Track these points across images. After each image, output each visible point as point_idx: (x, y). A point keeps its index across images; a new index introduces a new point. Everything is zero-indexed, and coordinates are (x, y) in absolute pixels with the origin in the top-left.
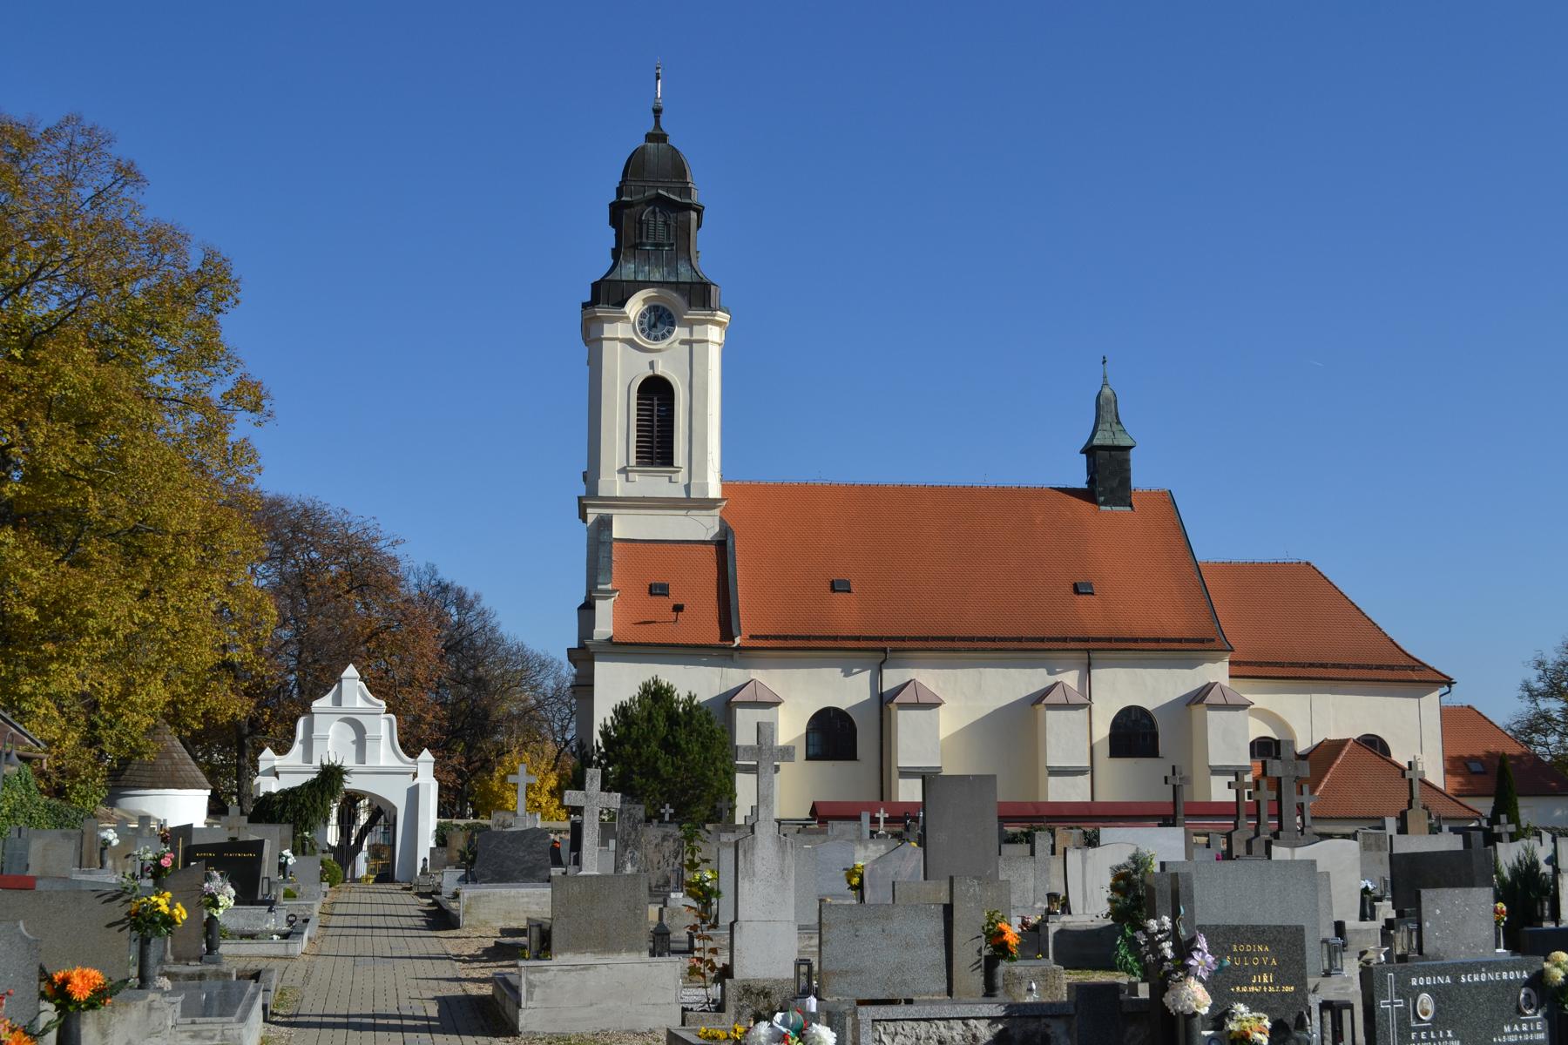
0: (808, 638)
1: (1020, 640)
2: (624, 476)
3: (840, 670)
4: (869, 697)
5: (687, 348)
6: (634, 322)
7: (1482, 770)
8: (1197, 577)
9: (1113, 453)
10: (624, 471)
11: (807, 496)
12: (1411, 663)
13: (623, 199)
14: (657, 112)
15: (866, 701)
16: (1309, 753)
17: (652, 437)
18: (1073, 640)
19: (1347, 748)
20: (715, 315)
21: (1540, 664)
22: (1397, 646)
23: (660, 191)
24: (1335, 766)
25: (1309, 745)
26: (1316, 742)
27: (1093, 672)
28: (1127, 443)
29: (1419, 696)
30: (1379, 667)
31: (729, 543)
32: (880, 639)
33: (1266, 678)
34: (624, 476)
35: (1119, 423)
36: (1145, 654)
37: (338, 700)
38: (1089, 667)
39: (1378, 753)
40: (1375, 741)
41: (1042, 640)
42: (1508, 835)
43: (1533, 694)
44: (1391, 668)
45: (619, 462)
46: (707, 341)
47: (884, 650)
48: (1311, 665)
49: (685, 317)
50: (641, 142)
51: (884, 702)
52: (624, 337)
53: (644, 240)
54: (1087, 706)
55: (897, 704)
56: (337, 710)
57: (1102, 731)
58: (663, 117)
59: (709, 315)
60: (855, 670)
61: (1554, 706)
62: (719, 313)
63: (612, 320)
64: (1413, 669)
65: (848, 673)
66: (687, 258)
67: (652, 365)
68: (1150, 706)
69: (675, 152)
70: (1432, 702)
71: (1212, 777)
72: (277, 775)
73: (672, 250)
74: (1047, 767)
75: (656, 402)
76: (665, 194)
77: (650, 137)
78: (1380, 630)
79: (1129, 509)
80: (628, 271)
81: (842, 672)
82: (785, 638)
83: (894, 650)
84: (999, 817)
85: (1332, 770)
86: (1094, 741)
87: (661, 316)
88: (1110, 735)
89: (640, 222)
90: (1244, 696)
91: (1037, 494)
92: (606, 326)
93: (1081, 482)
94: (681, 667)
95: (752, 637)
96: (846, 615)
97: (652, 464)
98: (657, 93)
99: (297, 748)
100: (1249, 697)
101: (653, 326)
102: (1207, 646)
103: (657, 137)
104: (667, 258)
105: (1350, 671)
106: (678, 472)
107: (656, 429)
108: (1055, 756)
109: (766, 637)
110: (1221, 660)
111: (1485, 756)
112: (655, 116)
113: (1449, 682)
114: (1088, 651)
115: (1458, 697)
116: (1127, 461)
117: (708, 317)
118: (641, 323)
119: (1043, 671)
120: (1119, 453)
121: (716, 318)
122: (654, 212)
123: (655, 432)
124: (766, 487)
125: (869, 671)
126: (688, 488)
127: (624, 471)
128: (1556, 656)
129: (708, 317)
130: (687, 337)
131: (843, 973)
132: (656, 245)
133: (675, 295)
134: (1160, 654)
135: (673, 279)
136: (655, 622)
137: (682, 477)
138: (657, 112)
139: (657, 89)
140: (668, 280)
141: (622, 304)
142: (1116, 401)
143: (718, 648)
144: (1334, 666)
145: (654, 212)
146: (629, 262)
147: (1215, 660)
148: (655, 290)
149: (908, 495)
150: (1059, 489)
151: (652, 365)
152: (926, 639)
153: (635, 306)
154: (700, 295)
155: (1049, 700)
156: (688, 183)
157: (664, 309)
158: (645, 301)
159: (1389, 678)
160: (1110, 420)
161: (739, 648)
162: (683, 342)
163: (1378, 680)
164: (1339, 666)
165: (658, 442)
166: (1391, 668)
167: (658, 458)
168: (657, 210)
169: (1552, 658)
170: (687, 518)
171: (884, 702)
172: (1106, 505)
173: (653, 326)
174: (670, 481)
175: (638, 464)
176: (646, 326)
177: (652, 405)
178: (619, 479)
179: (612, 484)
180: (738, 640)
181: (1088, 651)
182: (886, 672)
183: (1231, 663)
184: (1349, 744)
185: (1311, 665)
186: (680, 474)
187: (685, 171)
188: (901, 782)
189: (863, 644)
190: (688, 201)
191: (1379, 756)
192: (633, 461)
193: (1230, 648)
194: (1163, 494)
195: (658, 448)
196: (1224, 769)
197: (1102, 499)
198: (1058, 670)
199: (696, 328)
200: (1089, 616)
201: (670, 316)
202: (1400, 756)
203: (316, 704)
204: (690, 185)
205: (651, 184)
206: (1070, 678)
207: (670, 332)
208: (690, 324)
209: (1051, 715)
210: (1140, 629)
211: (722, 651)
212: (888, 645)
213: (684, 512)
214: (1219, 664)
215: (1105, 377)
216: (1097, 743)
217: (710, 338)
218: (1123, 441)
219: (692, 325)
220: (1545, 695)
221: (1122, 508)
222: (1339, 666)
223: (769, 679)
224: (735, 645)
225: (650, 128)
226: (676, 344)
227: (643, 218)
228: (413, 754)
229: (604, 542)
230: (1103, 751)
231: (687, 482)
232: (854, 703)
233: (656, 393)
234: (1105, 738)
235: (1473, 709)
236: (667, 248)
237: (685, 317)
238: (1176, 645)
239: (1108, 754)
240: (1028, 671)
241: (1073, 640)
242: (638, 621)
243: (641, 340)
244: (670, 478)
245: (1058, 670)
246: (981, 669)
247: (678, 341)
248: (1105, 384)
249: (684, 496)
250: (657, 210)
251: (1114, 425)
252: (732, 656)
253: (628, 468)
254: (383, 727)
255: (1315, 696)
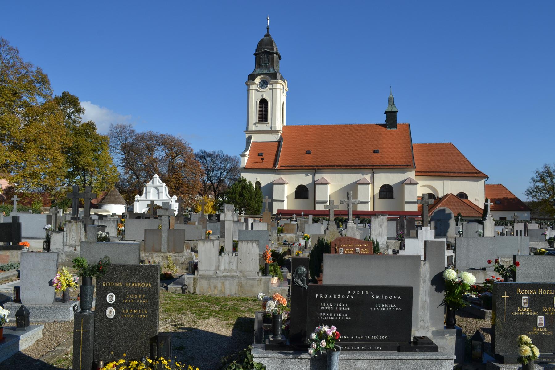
1: (354, 166)
5: (271, 90)
8: (411, 148)
10: (255, 124)
11: (306, 129)
14: (268, 29)
17: (262, 116)
18: (369, 166)
22: (473, 167)
23: (266, 50)
24: (443, 201)
26: (445, 195)
27: (374, 174)
29: (478, 181)
30: (465, 173)
31: (281, 142)
32: (315, 166)
33: (429, 176)
35: (394, 105)
36: (389, 170)
37: (153, 183)
38: (373, 173)
41: (360, 166)
42: (156, 227)
45: (254, 122)
47: (315, 169)
48: (444, 172)
50: (263, 37)
51: (315, 184)
53: (262, 63)
56: (153, 185)
57: (377, 191)
58: (269, 30)
63: (252, 84)
64: (476, 173)
65: (306, 175)
67: (262, 95)
68: (391, 184)
69: (271, 38)
70: (482, 183)
72: (139, 201)
75: (263, 105)
76: (267, 50)
77: (266, 36)
80: (258, 71)
82: (289, 166)
83: (317, 169)
84: (335, 214)
86: (374, 194)
88: (379, 192)
89: (261, 58)
91: (370, 126)
92: (250, 86)
93: (383, 122)
94: (263, 174)
95: (281, 166)
96: (308, 160)
97: (262, 122)
99: (144, 195)
100: (418, 181)
101: (262, 85)
102: (408, 167)
103: (267, 35)
105: (456, 174)
109: (284, 166)
110: (413, 171)
113: (487, 177)
114: (373, 169)
115: (491, 181)
116: (396, 115)
118: (259, 85)
119: (361, 174)
122: (264, 55)
124: (296, 127)
126: (271, 128)
127: (255, 124)
130: (271, 88)
133: (267, 77)
137: (270, 125)
138: (268, 29)
141: (254, 80)
142: (393, 99)
144: (451, 172)
147: (411, 171)
149: (333, 127)
153: (258, 80)
154: (274, 76)
155: (406, 182)
157: (265, 81)
161: (277, 169)
162: (270, 89)
163: (464, 177)
164: (453, 172)
171: (315, 184)
175: (259, 122)
176: (261, 85)
177: (262, 106)
178: (254, 126)
179: (252, 127)
180: (277, 167)
181: (373, 169)
182: (316, 175)
183: (416, 172)
185: (444, 172)
189: (310, 168)
192: (258, 121)
193: (415, 167)
194: (407, 124)
197: (388, 126)
199: (273, 85)
200: (376, 159)
203: (148, 184)
206: (368, 177)
207: (267, 87)
208: (272, 84)
209: (406, 186)
210: (390, 162)
211: (272, 170)
212: (316, 168)
213: (270, 134)
214: (412, 172)
217: (277, 87)
218: (395, 110)
220: (539, 181)
221: (394, 129)
222: (453, 172)
223: (284, 177)
225: (266, 33)
226: (268, 90)
228: (171, 196)
230: (377, 197)
232: (308, 183)
233: (263, 103)
238: (399, 167)
241: (369, 166)
243: (259, 89)
248: (391, 94)
251: (392, 105)
252: (275, 171)
254: (164, 189)
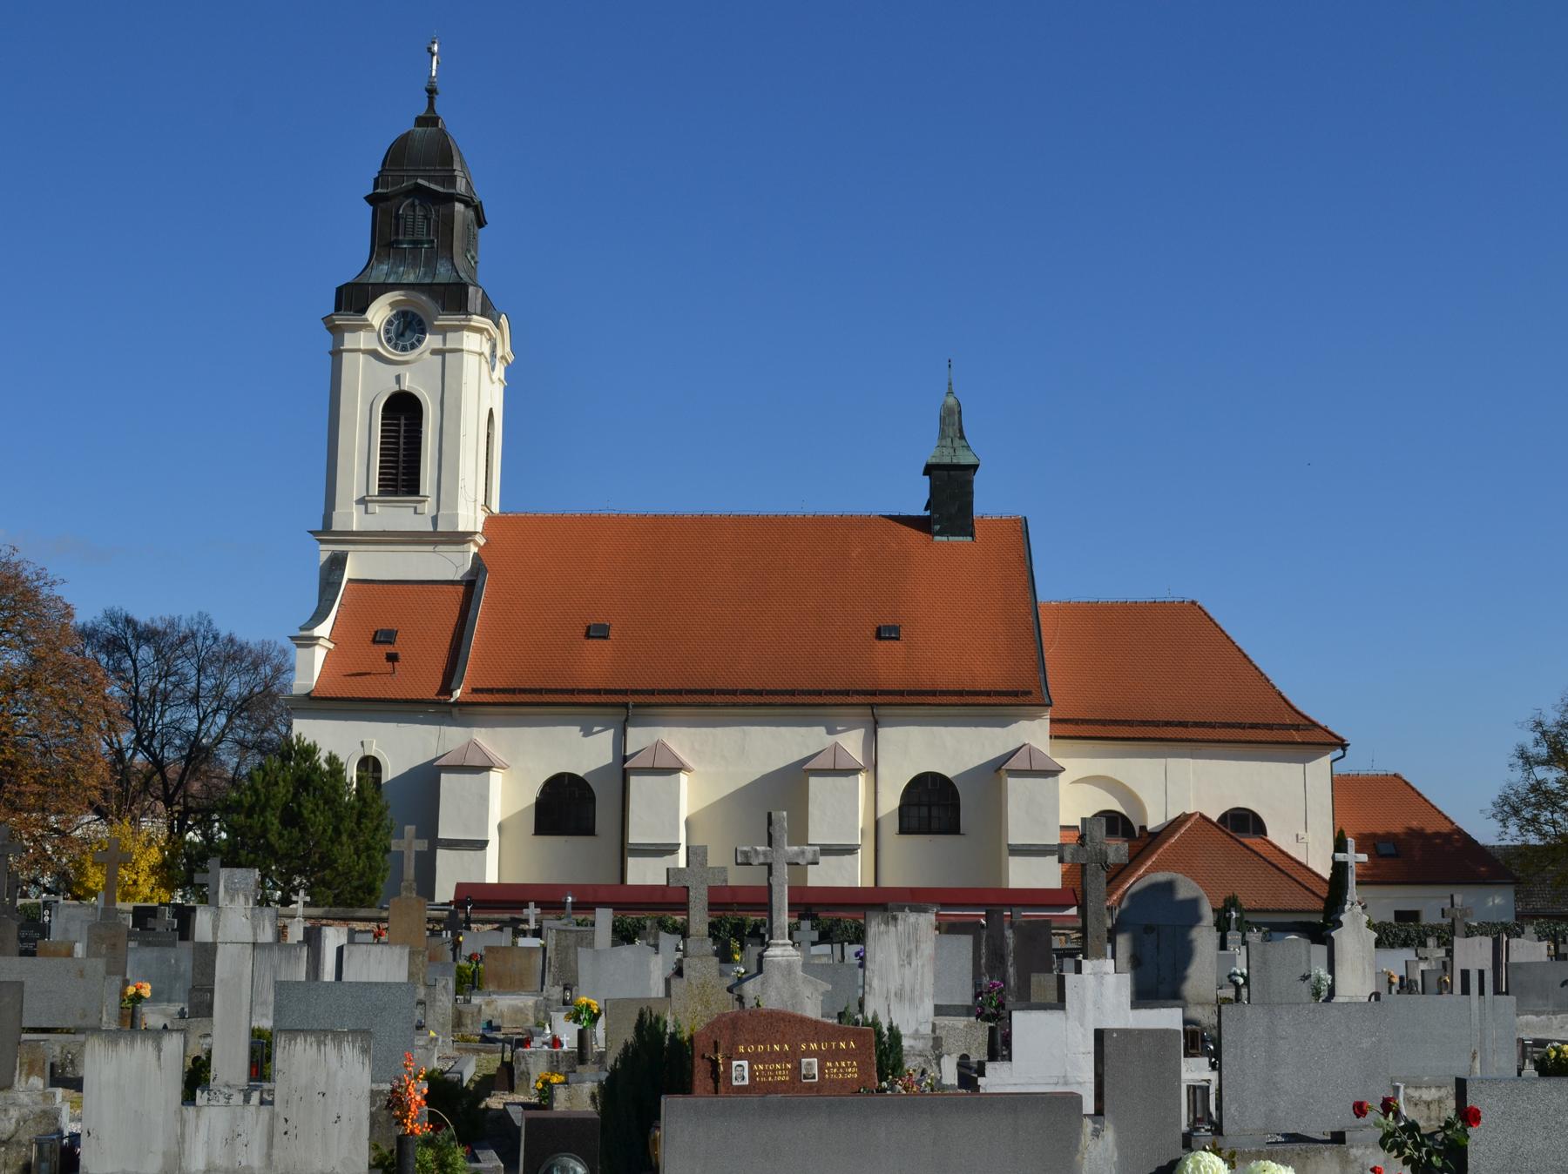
0: (540, 691)
2: (363, 507)
3: (579, 728)
4: (611, 761)
5: (438, 358)
6: (380, 329)
7: (1393, 851)
9: (952, 473)
10: (362, 501)
12: (1300, 721)
13: (379, 191)
14: (431, 92)
15: (609, 765)
16: (1161, 831)
18: (858, 693)
19: (1189, 825)
20: (470, 320)
21: (1539, 724)
23: (420, 181)
24: (1166, 846)
25: (1164, 821)
27: (882, 732)
28: (970, 460)
29: (1305, 761)
30: (1254, 726)
34: (363, 507)
35: (962, 437)
39: (1229, 832)
40: (1117, 818)
43: (1528, 761)
44: (1269, 727)
45: (357, 492)
46: (462, 350)
47: (626, 705)
49: (436, 323)
51: (622, 770)
52: (366, 348)
53: (401, 237)
54: (873, 767)
55: (1007, 770)
57: (890, 802)
59: (463, 320)
60: (596, 729)
61: (1550, 777)
62: (475, 317)
63: (355, 329)
64: (1297, 727)
65: (587, 733)
66: (449, 256)
67: (398, 379)
68: (950, 773)
69: (443, 134)
70: (1320, 769)
71: (1010, 858)
73: (433, 247)
74: (1009, 845)
77: (420, 121)
78: (1268, 681)
79: (969, 539)
80: (381, 273)
81: (581, 731)
83: (636, 706)
85: (1161, 850)
86: (880, 815)
87: (410, 323)
89: (397, 217)
90: (1055, 760)
92: (347, 336)
93: (918, 508)
95: (475, 691)
97: (396, 494)
98: (431, 71)
100: (1061, 762)
101: (400, 335)
102: (1021, 699)
103: (428, 120)
104: (426, 257)
106: (424, 501)
107: (402, 452)
108: (820, 832)
111: (1406, 834)
112: (429, 97)
113: (1343, 745)
114: (872, 706)
115: (1357, 762)
116: (971, 482)
117: (463, 323)
118: (387, 331)
119: (822, 730)
120: (959, 473)
121: (472, 323)
122: (413, 205)
123: (401, 456)
124: (543, 519)
125: (612, 731)
126: (435, 520)
127: (362, 501)
128: (1558, 717)
129: (463, 323)
131: (198, 1116)
132: (414, 242)
133: (424, 298)
134: (963, 710)
135: (427, 281)
136: (369, 674)
137: (428, 508)
138: (431, 92)
139: (431, 67)
140: (423, 282)
142: (960, 412)
143: (430, 703)
144: (1197, 725)
145: (413, 205)
146: (382, 263)
147: (1032, 717)
148: (402, 292)
149: (705, 523)
150: (891, 518)
151: (398, 379)
152: (679, 692)
153: (379, 312)
154: (454, 298)
156: (455, 170)
157: (414, 315)
158: (393, 305)
159: (1238, 738)
160: (951, 434)
161: (457, 703)
162: (434, 352)
165: (404, 468)
166: (1269, 727)
167: (403, 486)
168: (417, 202)
169: (1551, 718)
170: (434, 554)
171: (622, 770)
172: (942, 535)
173: (400, 335)
174: (416, 513)
175: (381, 493)
176: (392, 335)
177: (398, 425)
179: (351, 517)
180: (458, 693)
181: (872, 706)
183: (1052, 721)
184: (1193, 820)
185: (1167, 724)
186: (426, 503)
187: (452, 157)
188: (1011, 859)
189: (603, 699)
190: (453, 191)
191: (1228, 834)
192: (375, 490)
193: (1047, 701)
195: (404, 474)
196: (827, 848)
198: (839, 728)
199: (450, 335)
201: (421, 322)
202: (1277, 834)
204: (456, 173)
205: (411, 173)
206: (852, 742)
207: (420, 341)
208: (443, 331)
209: (1013, 784)
210: (947, 679)
212: (631, 700)
213: (430, 548)
215: (950, 384)
216: (882, 817)
217: (465, 347)
218: (965, 459)
219: (446, 332)
220: (1547, 762)
221: (961, 538)
223: (487, 739)
224: (452, 700)
225: (422, 110)
226: (427, 355)
227: (401, 212)
229: (334, 583)
230: (891, 827)
231: (435, 513)
234: (895, 810)
235: (1401, 778)
236: (426, 246)
237: (436, 323)
239: (533, 832)
240: (803, 730)
241: (858, 693)
242: (350, 673)
244: (415, 508)
245: (839, 728)
246: (745, 728)
247: (429, 351)
249: (431, 529)
250: (417, 202)
252: (450, 712)
253: (366, 498)
255: (1170, 760)
